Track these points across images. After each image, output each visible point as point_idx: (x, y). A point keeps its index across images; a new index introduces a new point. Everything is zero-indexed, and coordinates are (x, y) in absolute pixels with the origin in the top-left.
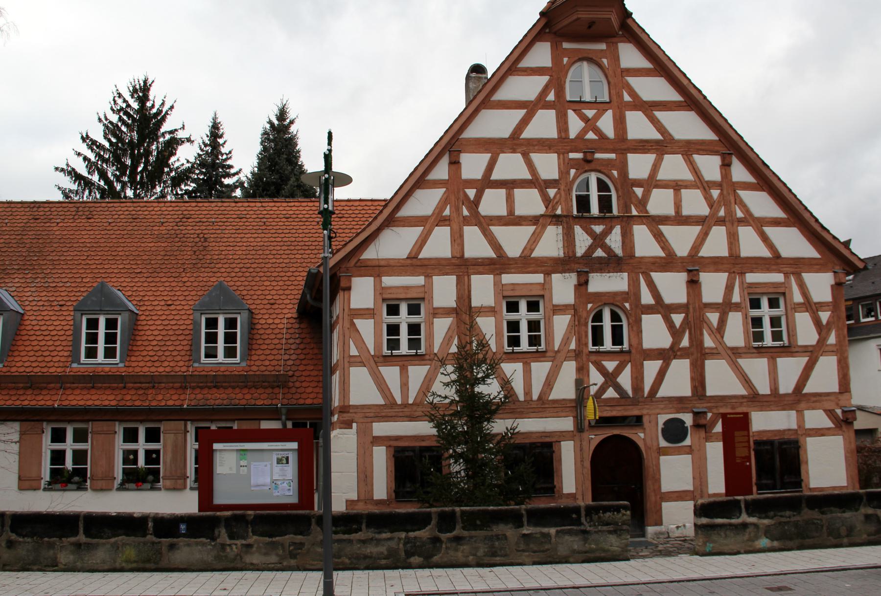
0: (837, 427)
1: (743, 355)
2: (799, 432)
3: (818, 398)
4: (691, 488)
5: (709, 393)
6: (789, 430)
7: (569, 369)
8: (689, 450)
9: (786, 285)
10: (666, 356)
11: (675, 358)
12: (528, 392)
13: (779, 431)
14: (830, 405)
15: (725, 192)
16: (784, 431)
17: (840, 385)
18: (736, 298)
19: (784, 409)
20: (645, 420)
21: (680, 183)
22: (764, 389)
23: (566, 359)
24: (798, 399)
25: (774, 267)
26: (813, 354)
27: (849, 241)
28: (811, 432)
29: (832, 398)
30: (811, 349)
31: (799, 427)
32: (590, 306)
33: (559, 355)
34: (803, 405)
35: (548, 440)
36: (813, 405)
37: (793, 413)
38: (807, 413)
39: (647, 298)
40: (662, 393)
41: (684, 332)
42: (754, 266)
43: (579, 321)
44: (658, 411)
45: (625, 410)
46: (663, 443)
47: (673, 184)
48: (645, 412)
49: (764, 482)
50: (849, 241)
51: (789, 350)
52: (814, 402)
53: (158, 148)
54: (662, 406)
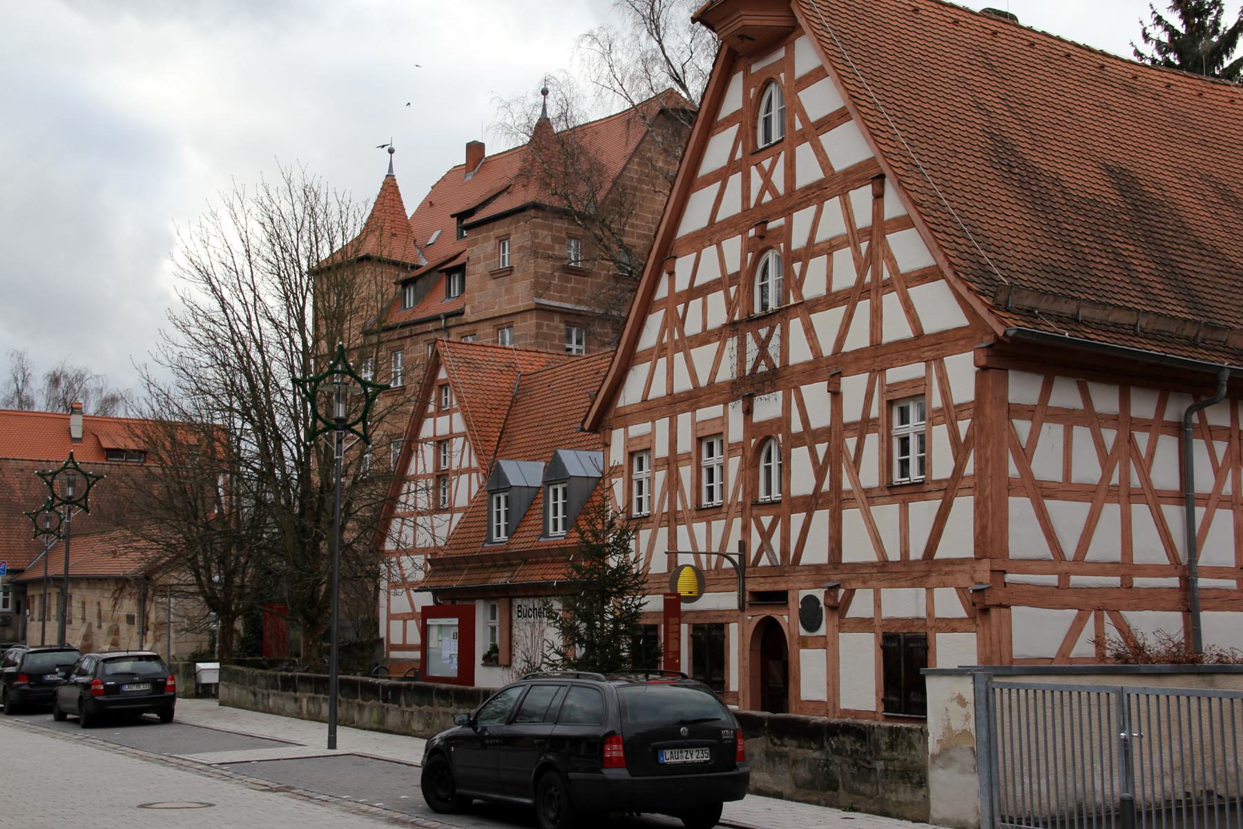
0: (972, 618)
1: (877, 500)
2: (928, 624)
4: (824, 698)
5: (844, 560)
6: (918, 619)
7: (964, 507)
8: (824, 643)
9: (924, 381)
10: (809, 504)
11: (816, 509)
12: (905, 553)
13: (907, 620)
14: (964, 580)
15: (874, 243)
16: (913, 620)
17: (976, 546)
18: (874, 412)
19: (913, 586)
20: (790, 595)
21: (834, 243)
22: (894, 555)
24: (925, 570)
25: (915, 354)
26: (948, 491)
27: (475, 150)
28: (942, 625)
29: (967, 567)
30: (945, 485)
34: (933, 579)
35: (720, 621)
38: (886, 593)
39: (796, 426)
40: (803, 561)
42: (894, 356)
44: (798, 585)
45: (775, 583)
46: (803, 632)
47: (826, 246)
48: (790, 585)
49: (891, 698)
50: (475, 150)
51: (918, 490)
52: (947, 574)
53: (218, 440)
54: (803, 578)
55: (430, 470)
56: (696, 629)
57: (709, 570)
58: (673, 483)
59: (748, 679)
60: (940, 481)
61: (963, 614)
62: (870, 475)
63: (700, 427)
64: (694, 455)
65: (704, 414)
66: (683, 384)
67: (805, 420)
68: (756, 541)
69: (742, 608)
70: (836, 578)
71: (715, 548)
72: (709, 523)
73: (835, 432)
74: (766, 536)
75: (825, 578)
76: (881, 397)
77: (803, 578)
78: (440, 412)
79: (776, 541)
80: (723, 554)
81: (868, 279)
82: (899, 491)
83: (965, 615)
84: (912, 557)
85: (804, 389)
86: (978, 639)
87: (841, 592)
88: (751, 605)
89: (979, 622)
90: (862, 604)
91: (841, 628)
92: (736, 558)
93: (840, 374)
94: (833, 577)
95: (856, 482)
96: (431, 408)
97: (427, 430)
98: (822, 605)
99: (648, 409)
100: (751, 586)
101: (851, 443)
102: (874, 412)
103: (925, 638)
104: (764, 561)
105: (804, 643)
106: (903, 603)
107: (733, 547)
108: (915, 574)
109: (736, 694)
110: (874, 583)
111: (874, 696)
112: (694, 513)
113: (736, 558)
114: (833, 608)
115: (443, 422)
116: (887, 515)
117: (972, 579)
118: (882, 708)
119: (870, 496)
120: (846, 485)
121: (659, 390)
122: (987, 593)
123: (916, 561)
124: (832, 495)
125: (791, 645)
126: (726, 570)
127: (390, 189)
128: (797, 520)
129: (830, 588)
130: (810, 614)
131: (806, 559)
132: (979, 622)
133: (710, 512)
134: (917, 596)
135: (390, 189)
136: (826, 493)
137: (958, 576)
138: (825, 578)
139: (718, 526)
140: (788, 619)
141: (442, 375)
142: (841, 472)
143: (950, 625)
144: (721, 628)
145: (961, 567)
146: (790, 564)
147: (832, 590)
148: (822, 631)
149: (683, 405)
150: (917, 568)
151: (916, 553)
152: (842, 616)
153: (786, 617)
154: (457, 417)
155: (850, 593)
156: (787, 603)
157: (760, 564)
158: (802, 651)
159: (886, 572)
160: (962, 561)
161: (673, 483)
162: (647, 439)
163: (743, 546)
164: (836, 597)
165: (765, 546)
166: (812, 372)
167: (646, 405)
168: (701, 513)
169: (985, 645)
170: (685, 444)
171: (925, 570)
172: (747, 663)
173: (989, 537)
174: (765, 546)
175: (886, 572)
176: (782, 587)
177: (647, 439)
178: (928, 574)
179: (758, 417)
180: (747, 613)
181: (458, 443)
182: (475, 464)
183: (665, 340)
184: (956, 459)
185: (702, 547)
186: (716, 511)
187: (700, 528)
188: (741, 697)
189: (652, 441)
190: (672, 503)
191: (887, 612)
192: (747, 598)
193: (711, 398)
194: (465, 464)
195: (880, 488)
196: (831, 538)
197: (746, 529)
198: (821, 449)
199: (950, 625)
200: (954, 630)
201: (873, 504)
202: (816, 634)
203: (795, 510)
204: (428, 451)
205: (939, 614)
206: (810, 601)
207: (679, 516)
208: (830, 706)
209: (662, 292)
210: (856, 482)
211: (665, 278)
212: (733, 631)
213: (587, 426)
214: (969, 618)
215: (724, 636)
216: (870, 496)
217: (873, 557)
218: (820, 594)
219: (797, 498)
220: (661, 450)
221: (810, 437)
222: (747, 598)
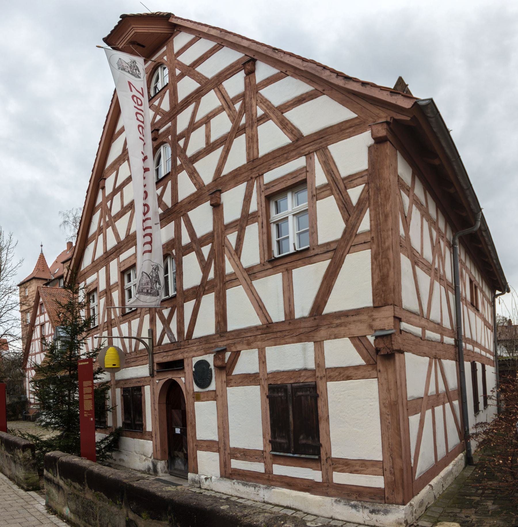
0: (371, 364)
2: (318, 374)
3: (343, 320)
4: (216, 439)
6: (306, 370)
7: (358, 265)
8: (214, 396)
10: (197, 293)
11: (204, 294)
13: (294, 372)
14: (359, 329)
16: (300, 371)
19: (300, 341)
22: (277, 315)
24: (318, 324)
26: (336, 254)
29: (364, 317)
30: (334, 246)
31: (318, 365)
34: (323, 332)
36: (336, 331)
37: (311, 346)
38: (271, 352)
39: (186, 239)
45: (174, 354)
46: (196, 389)
48: (186, 355)
51: (303, 257)
52: (338, 326)
54: (195, 348)
55: (39, 336)
56: (125, 391)
57: (130, 353)
58: (109, 302)
59: (158, 423)
60: (328, 244)
61: (361, 361)
62: (251, 255)
63: (122, 265)
64: (119, 283)
65: (123, 256)
66: (112, 243)
67: (192, 233)
68: (159, 327)
69: (152, 375)
70: (222, 344)
71: (134, 334)
73: (216, 237)
74: (166, 323)
75: (213, 345)
76: (259, 195)
77: (195, 348)
78: (41, 314)
79: (173, 326)
80: (139, 339)
81: (211, 275)
82: (278, 262)
83: (362, 362)
84: (297, 315)
85: (190, 214)
86: (380, 384)
87: (228, 354)
88: (158, 372)
89: (380, 367)
90: (247, 362)
91: (228, 383)
92: (147, 341)
93: (220, 192)
94: (220, 344)
95: (238, 265)
96: (38, 313)
97: (37, 323)
98: (212, 367)
99: (96, 266)
100: (158, 359)
101: (232, 238)
102: (253, 207)
103: (315, 387)
104: (166, 340)
105: (197, 397)
106: (290, 358)
107: (145, 334)
108: (301, 330)
109: (150, 433)
110: (259, 343)
111: (261, 438)
112: (121, 319)
113: (147, 341)
114: (220, 368)
115: (42, 317)
116: (270, 287)
117: (371, 327)
118: (269, 448)
119: (252, 273)
120: (229, 268)
121: (100, 252)
122: (392, 335)
123: (303, 319)
124: (217, 281)
125: (188, 399)
126: (141, 351)
127: (42, 258)
128: (189, 306)
129: (218, 352)
130: (202, 375)
131: (197, 333)
132: (380, 367)
133: (130, 315)
134: (304, 350)
135: (42, 258)
136: (212, 281)
137: (352, 326)
138: (213, 345)
139: (135, 323)
140: (185, 380)
141: (41, 300)
142: (223, 261)
143: (344, 374)
144: (139, 389)
145: (355, 318)
146: (186, 339)
147: (219, 354)
148: (213, 387)
149: (112, 256)
150: (303, 325)
151: (303, 308)
152: (229, 374)
153: (183, 379)
154: (46, 315)
155: (237, 354)
156: (183, 368)
157: (164, 342)
158: (197, 404)
159: (269, 332)
160: (357, 312)
161: (109, 302)
162: (95, 283)
163: (152, 332)
164: (224, 358)
165: (166, 329)
166: (194, 201)
167: (94, 264)
168: (125, 317)
169: (389, 390)
170: (115, 278)
171: (318, 324)
172: (157, 412)
173: (391, 285)
174: (166, 329)
175: (269, 332)
176: (180, 357)
177: (95, 283)
178: (317, 328)
180: (155, 378)
181: (47, 324)
182: (53, 332)
183: (102, 224)
184: (346, 221)
185: (126, 334)
186: (133, 313)
187: (124, 327)
188: (154, 435)
189: (98, 283)
190: (109, 315)
191: (271, 367)
192: (155, 368)
193: (127, 245)
194: (50, 333)
195: (262, 264)
196: (217, 314)
197: (152, 321)
198: (206, 250)
199: (344, 374)
200: (349, 378)
201: (256, 278)
202: (207, 389)
203: (187, 299)
204: (38, 329)
205: (329, 364)
206: (202, 365)
207: (113, 322)
208: (221, 445)
209: (100, 200)
210: (238, 265)
211: (101, 191)
212: (147, 390)
214: (368, 364)
215: (141, 395)
216: (252, 273)
217: (256, 321)
218: (210, 359)
219: (188, 290)
220: (102, 286)
221: (197, 243)
222: (155, 368)
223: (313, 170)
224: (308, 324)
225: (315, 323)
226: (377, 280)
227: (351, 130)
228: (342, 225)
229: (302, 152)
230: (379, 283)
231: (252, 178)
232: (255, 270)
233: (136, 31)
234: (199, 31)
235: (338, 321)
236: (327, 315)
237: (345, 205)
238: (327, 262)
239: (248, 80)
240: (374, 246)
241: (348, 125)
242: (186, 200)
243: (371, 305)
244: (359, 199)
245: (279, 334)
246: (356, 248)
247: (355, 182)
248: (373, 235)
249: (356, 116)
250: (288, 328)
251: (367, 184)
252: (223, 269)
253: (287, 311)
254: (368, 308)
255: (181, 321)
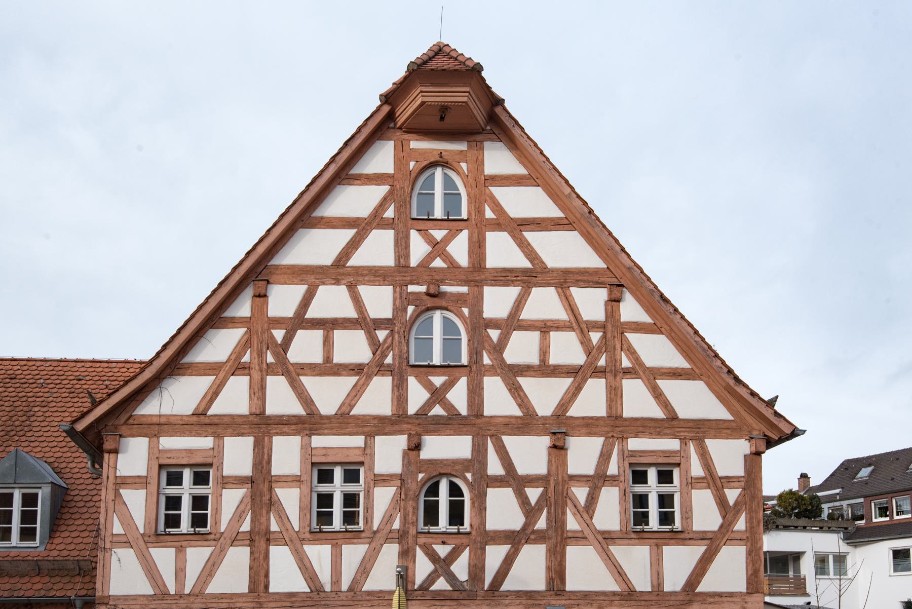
1: (618, 541)
3: (717, 599)
23: (387, 540)
32: (421, 476)
33: (378, 535)
39: (495, 467)
41: (540, 510)
43: (406, 495)
47: (542, 324)
72: (180, 551)
84: (667, 588)
93: (565, 434)
108: (671, 603)
142: (564, 513)
160: (731, 595)
179: (426, 454)
184: (724, 517)
213: (80, 427)
223: (688, 458)
224: (681, 598)
225: (688, 598)
226: (750, 572)
227: (728, 431)
228: (720, 520)
229: (678, 434)
230: (752, 575)
231: (613, 436)
232: (614, 536)
233: (425, 99)
234: (540, 172)
235: (712, 600)
236: (701, 593)
237: (722, 502)
238: (703, 548)
239: (609, 308)
240: (749, 544)
241: (725, 425)
242: (501, 419)
243: (744, 590)
244: (736, 501)
245: (643, 603)
246: (733, 542)
247: (732, 484)
248: (748, 535)
249: (732, 418)
250: (654, 598)
251: (744, 489)
252: (563, 523)
253: (655, 583)
254: (741, 593)
255: (476, 390)
